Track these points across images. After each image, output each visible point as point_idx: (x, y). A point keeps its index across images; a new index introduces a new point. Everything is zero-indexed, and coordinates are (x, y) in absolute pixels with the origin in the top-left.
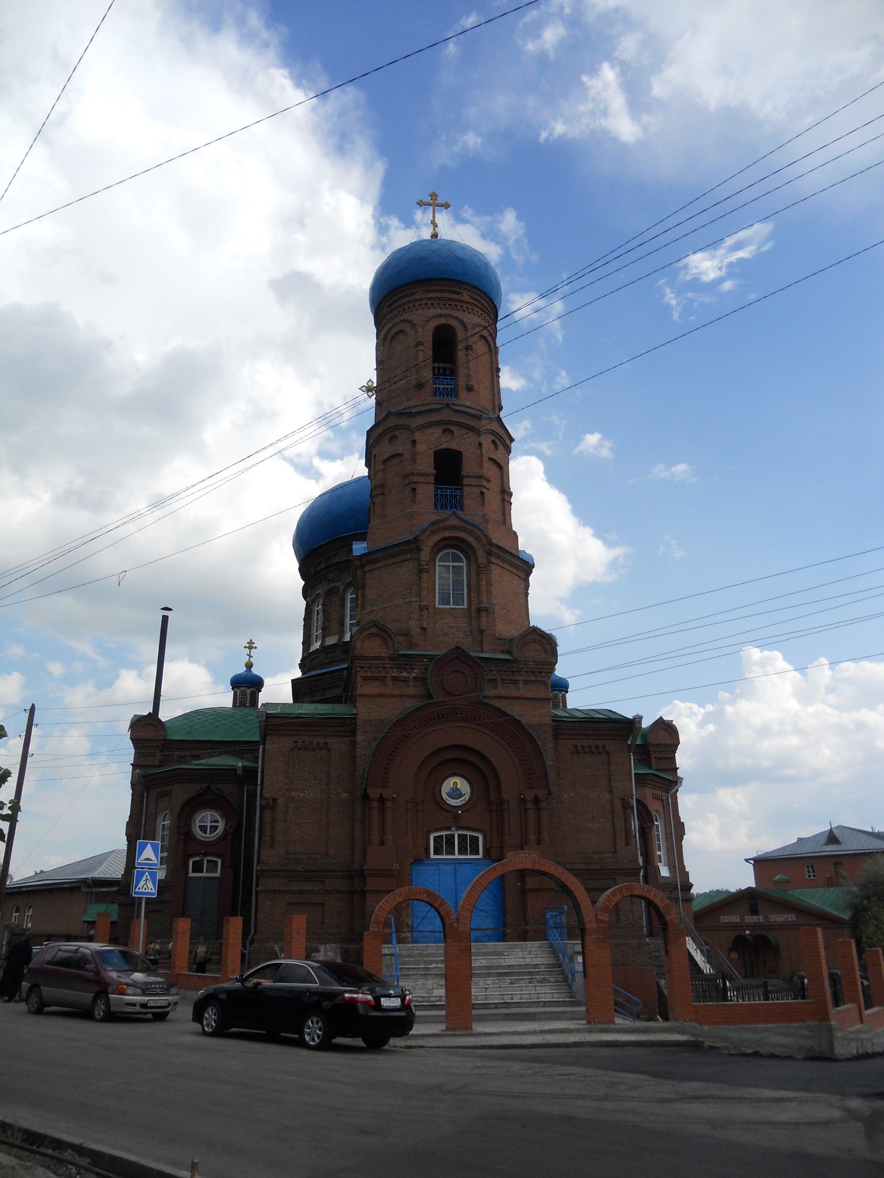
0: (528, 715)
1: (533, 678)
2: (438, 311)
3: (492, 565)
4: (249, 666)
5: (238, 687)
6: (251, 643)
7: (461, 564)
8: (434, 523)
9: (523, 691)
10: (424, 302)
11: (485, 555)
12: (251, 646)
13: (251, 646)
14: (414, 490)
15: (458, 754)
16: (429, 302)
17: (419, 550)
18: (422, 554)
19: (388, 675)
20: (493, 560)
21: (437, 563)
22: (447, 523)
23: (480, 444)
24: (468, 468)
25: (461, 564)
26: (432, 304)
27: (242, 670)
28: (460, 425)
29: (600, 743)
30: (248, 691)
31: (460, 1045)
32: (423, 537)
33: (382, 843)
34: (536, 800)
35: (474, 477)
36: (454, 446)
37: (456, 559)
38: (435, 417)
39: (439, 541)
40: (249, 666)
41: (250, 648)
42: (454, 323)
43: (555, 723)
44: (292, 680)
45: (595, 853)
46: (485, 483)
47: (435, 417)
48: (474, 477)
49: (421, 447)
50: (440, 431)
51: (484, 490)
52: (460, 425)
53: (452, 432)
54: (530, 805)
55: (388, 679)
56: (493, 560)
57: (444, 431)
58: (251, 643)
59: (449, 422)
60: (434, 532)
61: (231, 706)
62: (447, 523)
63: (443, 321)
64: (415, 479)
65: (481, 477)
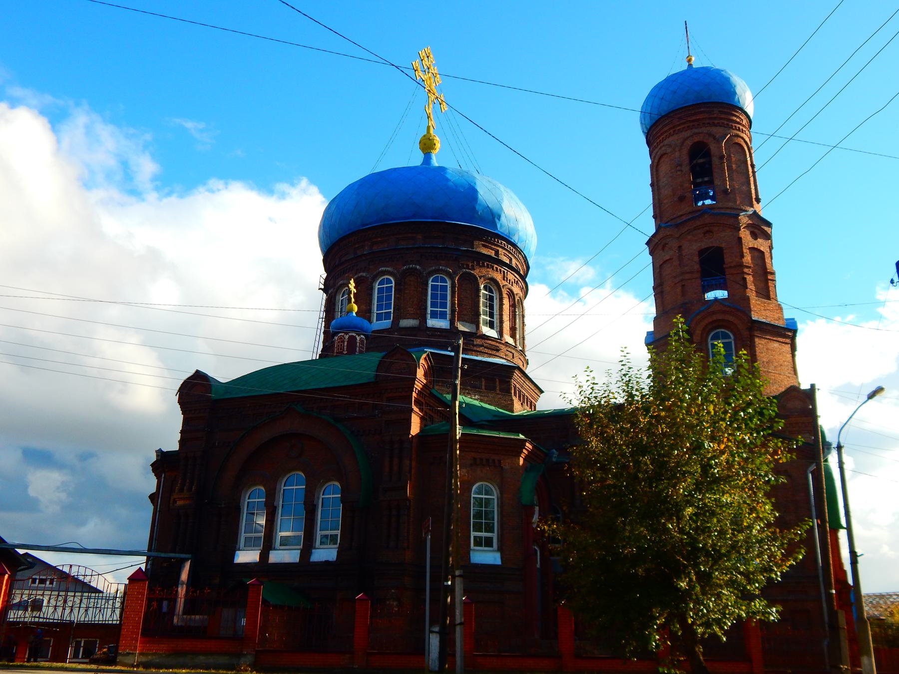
18: (865, 660)
63: (697, 139)
64: (687, 276)
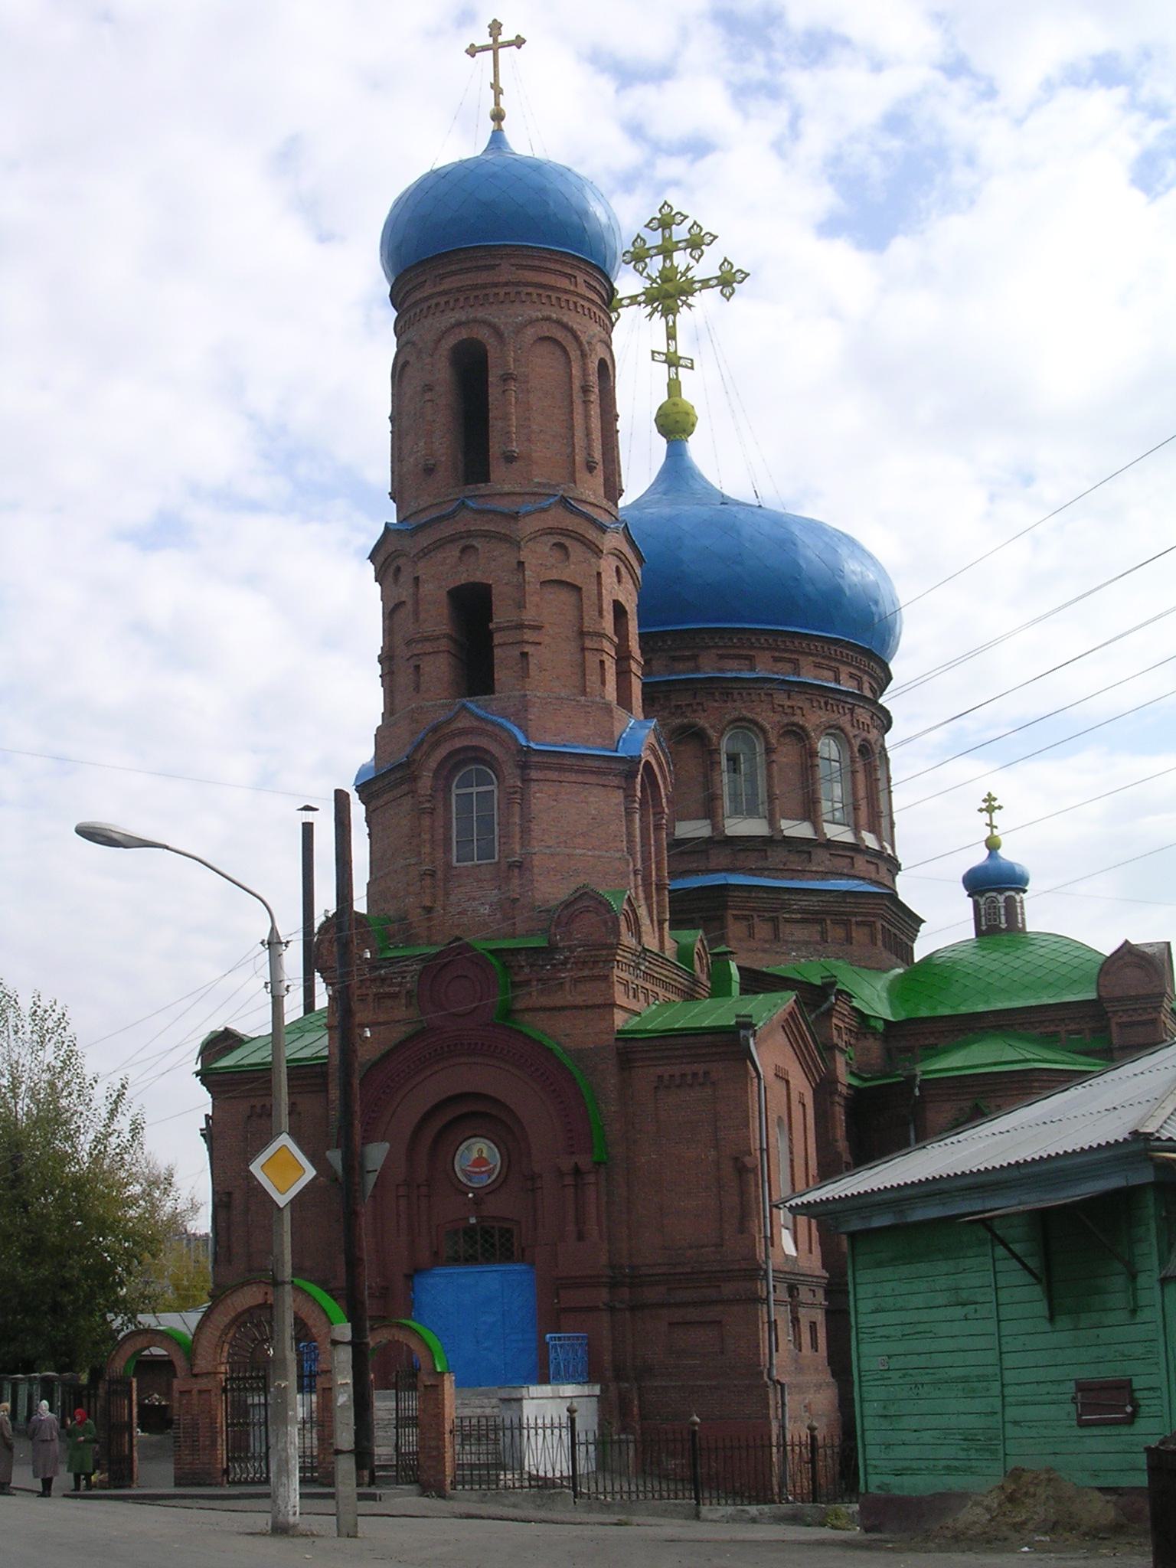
0: (564, 1034)
1: (586, 973)
2: (453, 317)
3: (533, 784)
4: (992, 845)
5: (981, 893)
6: (990, 798)
7: (490, 788)
8: (435, 729)
9: (569, 997)
10: (433, 302)
11: (518, 772)
12: (990, 805)
13: (990, 805)
14: (417, 667)
15: (448, 1115)
16: (443, 300)
17: (414, 779)
19: (369, 992)
20: (534, 774)
21: (455, 791)
22: (453, 726)
23: (521, 564)
24: (502, 614)
25: (490, 788)
26: (447, 303)
27: (979, 856)
28: (486, 535)
29: (700, 1068)
30: (1001, 898)
31: (789, 1169)
32: (418, 757)
33: (581, 1237)
34: (577, 1172)
35: (509, 628)
36: (478, 577)
37: (483, 780)
38: (446, 530)
39: (450, 755)
40: (992, 845)
41: (990, 810)
42: (483, 334)
43: (621, 1044)
44: (493, 693)
45: (691, 1248)
46: (529, 635)
47: (446, 530)
48: (509, 628)
49: (427, 589)
50: (457, 553)
51: (527, 649)
52: (486, 535)
53: (473, 547)
54: (569, 1180)
55: (370, 999)
56: (534, 774)
57: (465, 550)
58: (990, 798)
59: (469, 534)
60: (436, 745)
61: (971, 934)
62: (453, 726)
63: (464, 334)
65: (521, 626)
